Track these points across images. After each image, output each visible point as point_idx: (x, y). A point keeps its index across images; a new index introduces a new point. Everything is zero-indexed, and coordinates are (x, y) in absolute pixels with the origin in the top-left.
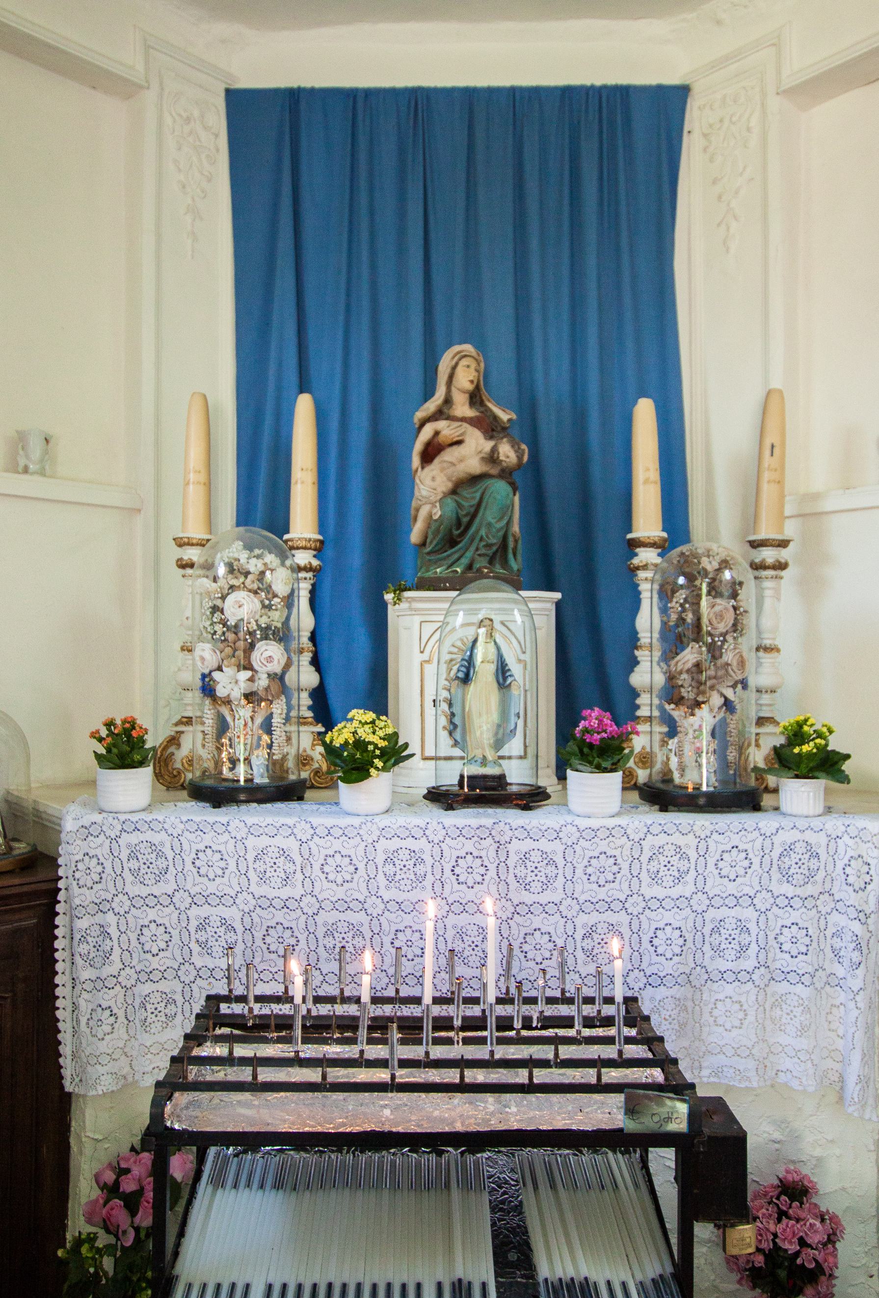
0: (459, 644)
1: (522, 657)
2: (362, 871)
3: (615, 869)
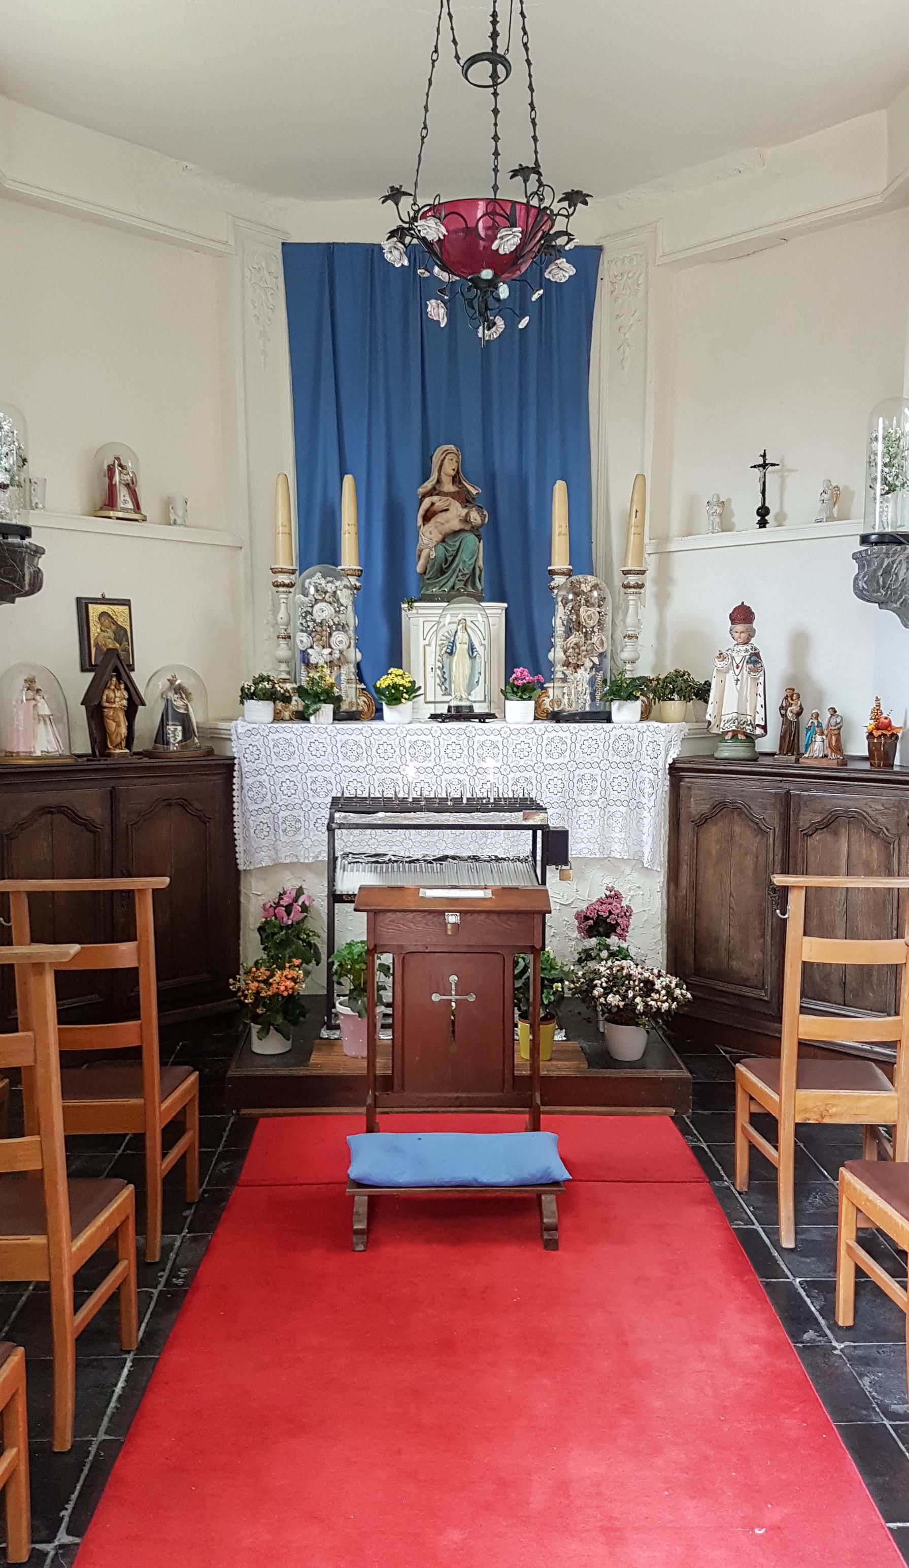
0: (446, 634)
2: (397, 752)
3: (529, 750)
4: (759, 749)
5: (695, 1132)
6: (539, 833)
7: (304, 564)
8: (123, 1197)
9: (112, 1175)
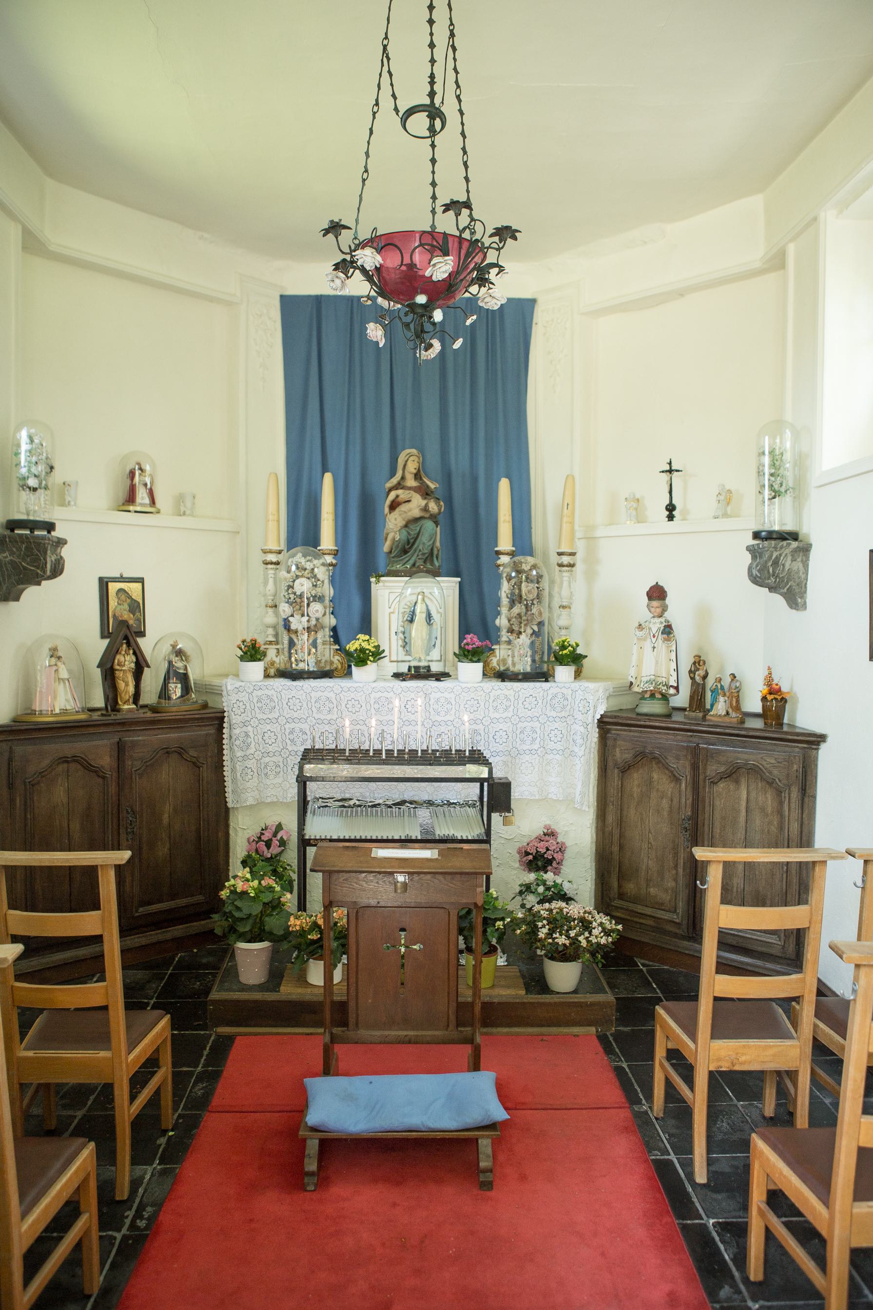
1: (440, 610)
4: (672, 704)
5: (617, 1050)
6: (486, 784)
7: (291, 544)
8: (81, 1160)
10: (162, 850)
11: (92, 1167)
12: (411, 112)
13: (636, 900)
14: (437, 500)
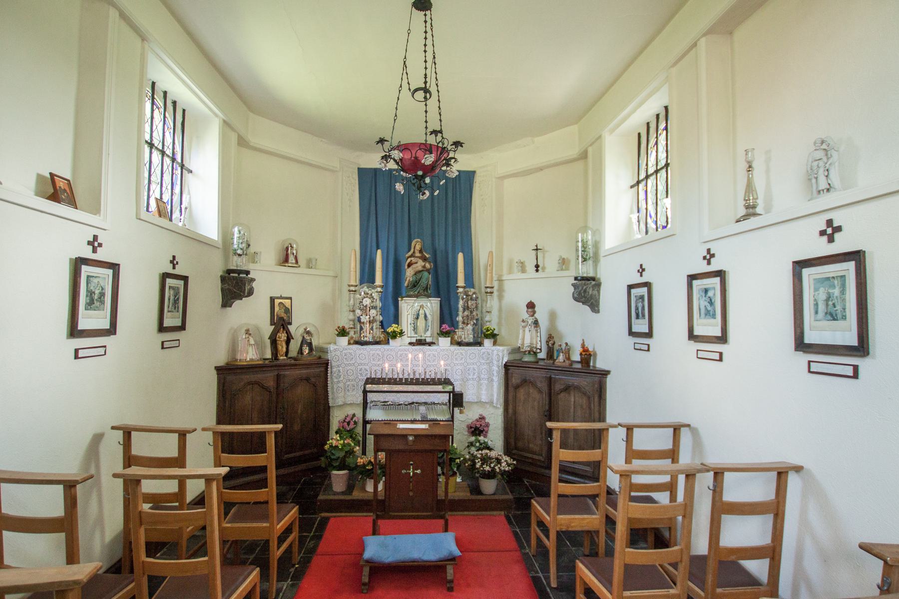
7: (362, 282)
9: (251, 564)
10: (296, 427)
11: (258, 580)
12: (416, 90)
13: (523, 450)
14: (430, 262)
